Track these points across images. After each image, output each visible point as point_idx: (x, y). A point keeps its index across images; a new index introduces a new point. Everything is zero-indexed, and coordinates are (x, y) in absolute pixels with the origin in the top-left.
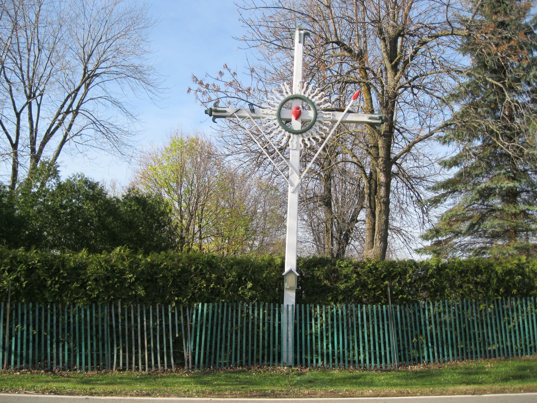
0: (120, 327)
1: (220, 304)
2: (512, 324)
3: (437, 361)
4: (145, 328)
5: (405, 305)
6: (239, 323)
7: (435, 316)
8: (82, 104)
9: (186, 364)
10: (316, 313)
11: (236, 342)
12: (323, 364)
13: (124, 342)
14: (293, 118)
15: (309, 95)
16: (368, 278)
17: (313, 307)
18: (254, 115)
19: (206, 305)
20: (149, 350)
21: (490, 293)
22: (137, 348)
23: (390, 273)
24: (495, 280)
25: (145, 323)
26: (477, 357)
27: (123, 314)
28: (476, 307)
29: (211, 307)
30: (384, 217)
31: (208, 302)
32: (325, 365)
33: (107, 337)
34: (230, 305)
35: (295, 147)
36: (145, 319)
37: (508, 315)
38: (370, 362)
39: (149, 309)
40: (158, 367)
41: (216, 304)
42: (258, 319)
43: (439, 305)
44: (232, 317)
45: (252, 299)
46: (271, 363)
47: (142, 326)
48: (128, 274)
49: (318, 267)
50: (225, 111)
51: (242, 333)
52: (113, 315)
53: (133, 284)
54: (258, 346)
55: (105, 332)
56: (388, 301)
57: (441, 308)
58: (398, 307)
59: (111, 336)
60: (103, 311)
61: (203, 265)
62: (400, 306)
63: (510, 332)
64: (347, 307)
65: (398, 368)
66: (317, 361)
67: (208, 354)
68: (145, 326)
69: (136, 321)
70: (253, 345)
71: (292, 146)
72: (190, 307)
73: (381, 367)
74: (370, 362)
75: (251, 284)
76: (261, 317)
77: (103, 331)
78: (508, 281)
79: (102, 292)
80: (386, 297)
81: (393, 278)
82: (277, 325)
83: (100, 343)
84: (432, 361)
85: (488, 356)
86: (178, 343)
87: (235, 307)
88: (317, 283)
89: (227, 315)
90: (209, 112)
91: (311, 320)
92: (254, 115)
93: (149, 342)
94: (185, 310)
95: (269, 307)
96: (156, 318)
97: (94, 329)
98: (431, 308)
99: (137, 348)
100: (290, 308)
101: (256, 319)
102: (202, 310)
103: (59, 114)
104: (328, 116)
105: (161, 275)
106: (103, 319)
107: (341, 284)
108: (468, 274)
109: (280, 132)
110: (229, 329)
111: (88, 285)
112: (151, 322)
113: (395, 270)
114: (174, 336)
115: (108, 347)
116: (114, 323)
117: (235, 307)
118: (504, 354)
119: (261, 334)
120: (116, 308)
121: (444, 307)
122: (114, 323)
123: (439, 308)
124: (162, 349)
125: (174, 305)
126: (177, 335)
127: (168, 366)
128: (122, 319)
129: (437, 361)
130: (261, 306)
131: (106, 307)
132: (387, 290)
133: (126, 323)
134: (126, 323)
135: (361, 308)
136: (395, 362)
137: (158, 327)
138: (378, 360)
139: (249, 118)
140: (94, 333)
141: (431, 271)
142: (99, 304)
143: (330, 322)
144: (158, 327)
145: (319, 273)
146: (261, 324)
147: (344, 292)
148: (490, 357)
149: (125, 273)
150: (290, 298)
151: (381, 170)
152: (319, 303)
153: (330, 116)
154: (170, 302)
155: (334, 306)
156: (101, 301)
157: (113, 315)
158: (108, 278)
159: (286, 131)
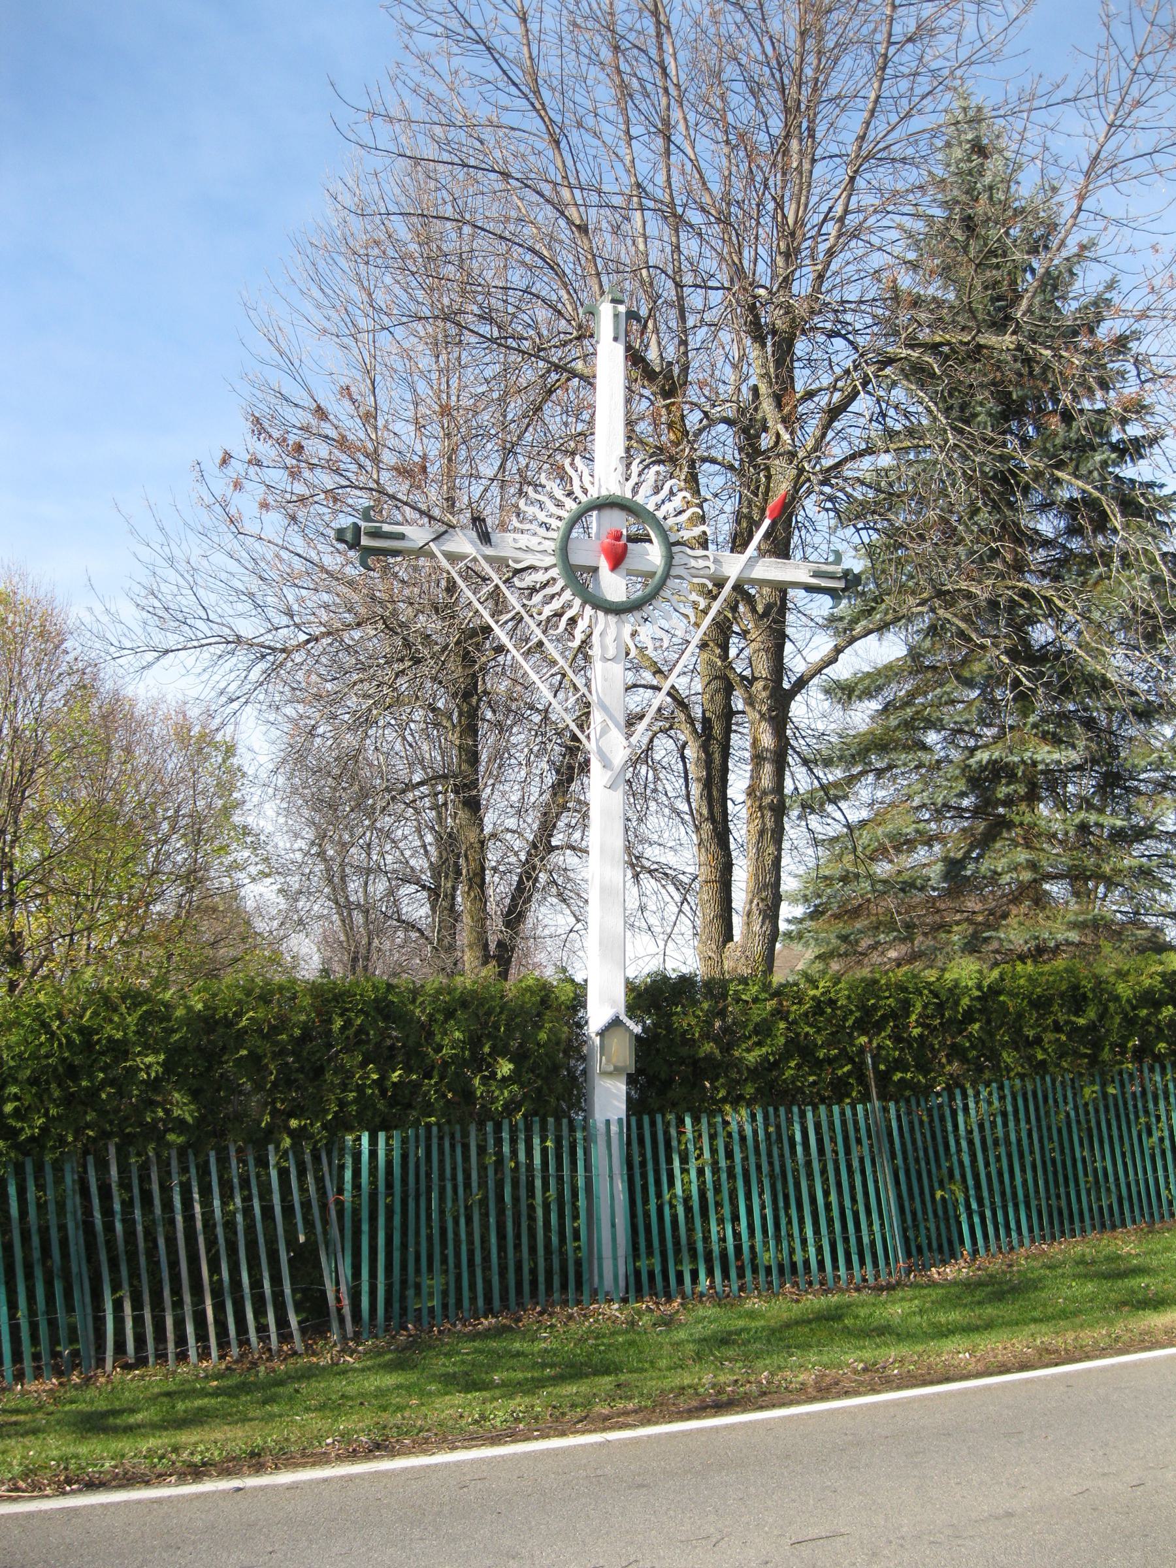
0: (119, 1226)
1: (422, 1131)
2: (1156, 1135)
3: (993, 1248)
4: (199, 1225)
5: (908, 1101)
6: (474, 1184)
7: (981, 1126)
9: (335, 1325)
11: (470, 1242)
12: (712, 1287)
13: (134, 1274)
14: (604, 565)
16: (819, 1031)
17: (673, 1123)
18: (489, 551)
19: (382, 1136)
20: (217, 1293)
21: (1106, 1055)
22: (176, 1291)
23: (868, 1012)
24: (1118, 1020)
25: (197, 1208)
26: (1083, 1230)
27: (125, 1185)
28: (1075, 1095)
29: (396, 1143)
30: (771, 849)
31: (387, 1128)
32: (719, 1288)
33: (78, 1265)
34: (446, 1128)
35: (611, 653)
36: (196, 1196)
37: (1147, 1112)
38: (836, 1267)
39: (207, 1162)
40: (248, 1342)
42: (530, 1166)
43: (990, 1094)
45: (511, 1107)
46: (571, 1294)
47: (189, 1218)
48: (139, 1054)
50: (402, 537)
51: (485, 1216)
52: (94, 1190)
53: (154, 1085)
54: (533, 1249)
55: (72, 1249)
56: (867, 1088)
57: (996, 1104)
58: (892, 1105)
59: (89, 1261)
60: (59, 1181)
61: (367, 1014)
62: (897, 1102)
63: (1153, 1157)
65: (908, 1275)
66: (695, 1275)
67: (397, 1287)
68: (198, 1216)
69: (168, 1206)
70: (517, 1247)
71: (604, 647)
72: (334, 1145)
73: (865, 1280)
74: (836, 1267)
75: (511, 1066)
76: (537, 1160)
77: (64, 1243)
78: (1147, 1022)
79: (59, 1118)
80: (862, 1079)
81: (879, 1026)
82: (581, 1183)
83: (58, 1287)
84: (982, 1251)
85: (1108, 1223)
86: (306, 1262)
87: (458, 1136)
88: (684, 1051)
89: (441, 1161)
90: (349, 537)
91: (669, 1161)
92: (489, 551)
93: (214, 1268)
94: (317, 1159)
96: (232, 1189)
97: (36, 1241)
98: (972, 1105)
99: (176, 1291)
100: (614, 1128)
101: (523, 1169)
102: (373, 1154)
104: (701, 563)
105: (244, 1052)
106: (61, 1206)
107: (748, 1050)
108: (1055, 1008)
110: (449, 1204)
111: (9, 1100)
112: (217, 1203)
113: (882, 1003)
114: (291, 1242)
115: (82, 1296)
116: (97, 1215)
117: (458, 1136)
118: (1143, 1216)
119: (540, 1212)
120: (102, 1166)
121: (1002, 1098)
122: (97, 1215)
123: (990, 1103)
124: (256, 1284)
125: (287, 1142)
126: (302, 1239)
127: (279, 1335)
128: (123, 1203)
129: (993, 1248)
130: (536, 1128)
131: (67, 1167)
132: (863, 1062)
133: (138, 1213)
134: (138, 1213)
135: (803, 1115)
136: (897, 1261)
137: (239, 1218)
138: (855, 1258)
140: (36, 1254)
141: (965, 1001)
142: (48, 1158)
143: (723, 1163)
144: (239, 1218)
145: (687, 1021)
146: (538, 1183)
147: (755, 1073)
148: (1114, 1227)
149: (126, 1052)
151: (762, 716)
152: (689, 1110)
153: (707, 563)
154: (270, 1135)
156: (54, 1148)
157: (94, 1190)
158: (73, 1072)
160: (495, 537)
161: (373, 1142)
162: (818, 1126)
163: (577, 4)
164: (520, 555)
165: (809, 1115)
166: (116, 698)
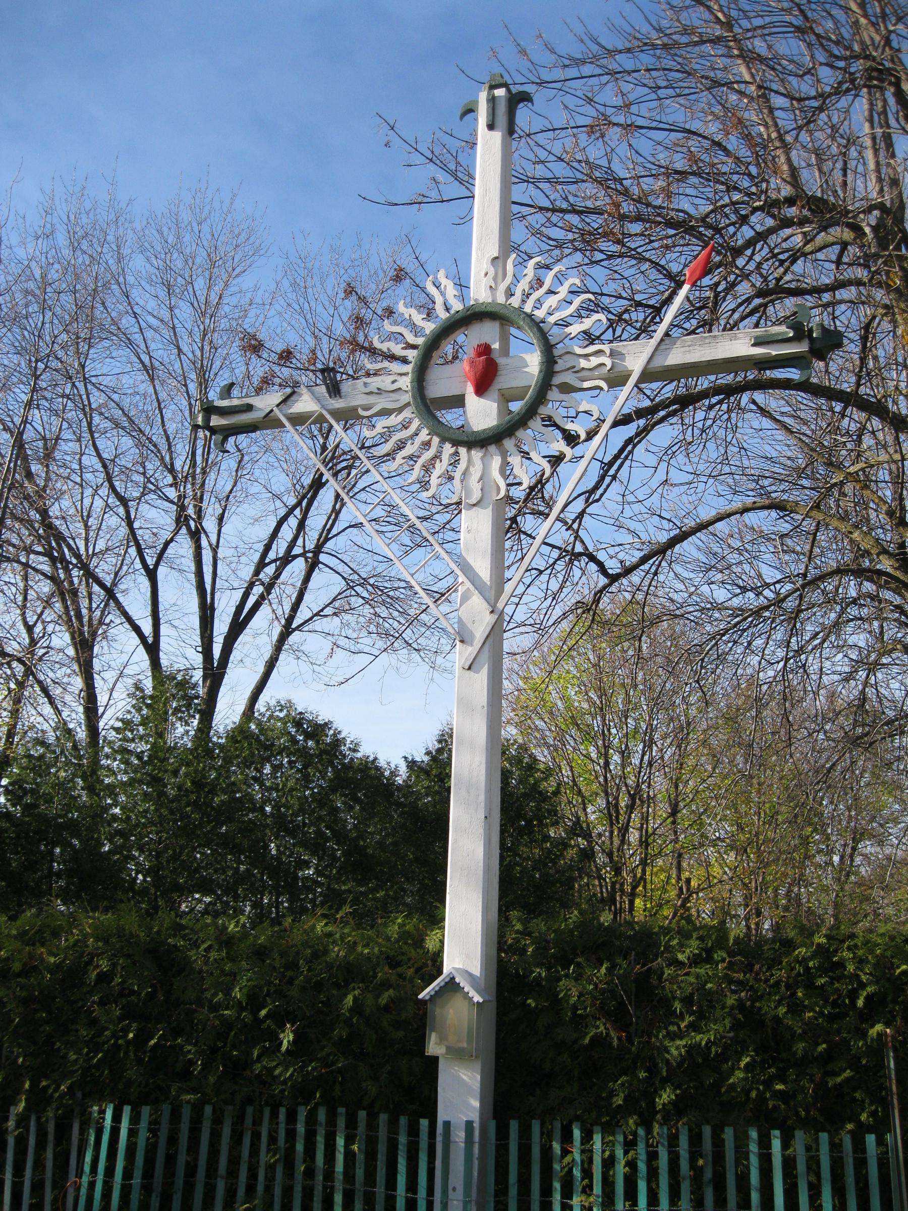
6: (260, 1188)
8: (327, 539)
10: (568, 1159)
15: (524, 302)
41: (166, 1108)
44: (234, 1162)
45: (303, 1092)
49: (579, 965)
64: (695, 1139)
76: (339, 1166)
95: (372, 1126)
103: (261, 565)
104: (595, 361)
109: (427, 445)
130: (341, 1122)
132: (881, 1066)
139: (321, 419)
150: (462, 1094)
155: (641, 1132)
159: (443, 440)
160: (345, 387)
161: (117, 1118)
162: (789, 1164)
163: (862, 6)
164: (371, 399)
165: (776, 1144)
166: (337, 732)
